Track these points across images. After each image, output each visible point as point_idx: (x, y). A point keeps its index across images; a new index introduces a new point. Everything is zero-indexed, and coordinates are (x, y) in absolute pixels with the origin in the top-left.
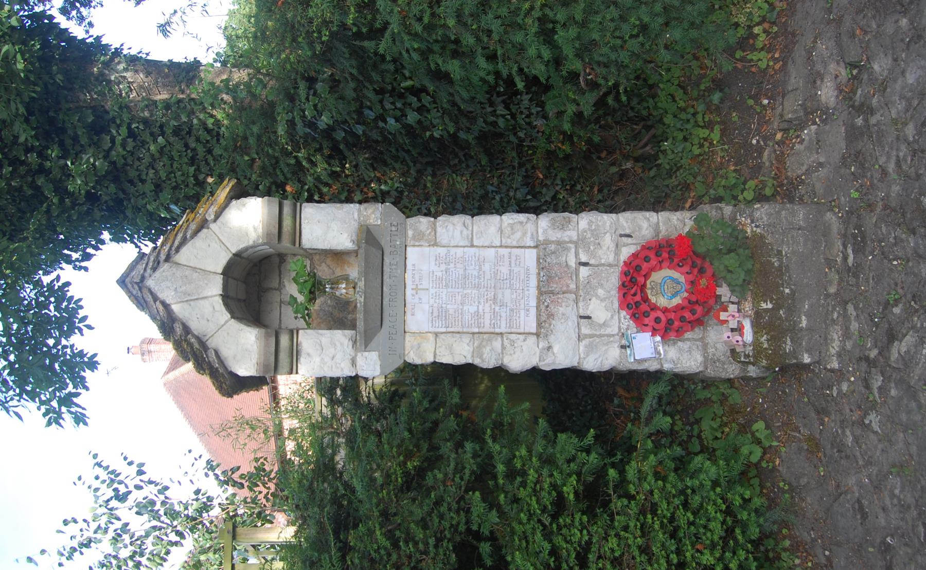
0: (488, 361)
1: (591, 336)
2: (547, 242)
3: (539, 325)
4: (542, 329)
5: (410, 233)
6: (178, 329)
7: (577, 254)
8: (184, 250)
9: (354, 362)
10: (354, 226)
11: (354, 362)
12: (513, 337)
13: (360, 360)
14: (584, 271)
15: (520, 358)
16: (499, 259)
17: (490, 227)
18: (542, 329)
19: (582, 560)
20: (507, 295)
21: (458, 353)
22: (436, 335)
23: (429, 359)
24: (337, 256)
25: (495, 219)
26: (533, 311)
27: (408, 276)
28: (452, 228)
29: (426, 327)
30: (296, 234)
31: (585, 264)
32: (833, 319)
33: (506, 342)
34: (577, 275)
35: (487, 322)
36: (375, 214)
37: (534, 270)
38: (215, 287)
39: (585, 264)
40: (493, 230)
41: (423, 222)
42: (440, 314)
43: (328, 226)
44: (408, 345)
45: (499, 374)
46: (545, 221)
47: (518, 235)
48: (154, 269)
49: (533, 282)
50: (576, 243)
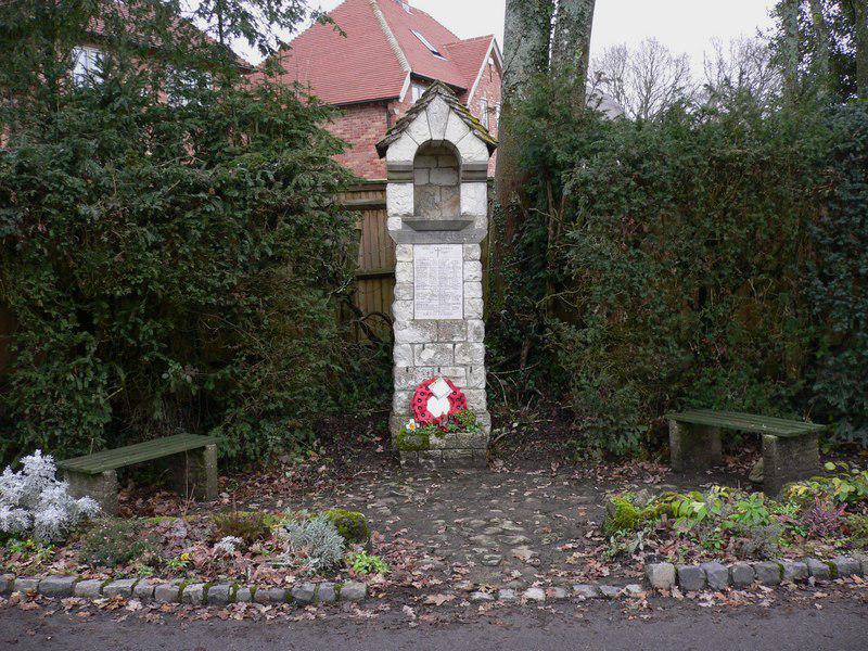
0: (399, 291)
1: (413, 350)
2: (467, 324)
3: (418, 321)
4: (415, 323)
5: (470, 246)
6: (414, 116)
7: (460, 342)
8: (457, 117)
9: (395, 215)
10: (474, 212)
11: (395, 215)
12: (412, 306)
13: (396, 219)
14: (450, 346)
15: (401, 311)
16: (457, 298)
17: (475, 292)
18: (415, 323)
19: (864, 378)
20: (435, 303)
21: (402, 276)
22: (412, 262)
23: (481, 300)
24: (457, 202)
25: (480, 294)
26: (427, 317)
27: (446, 246)
28: (474, 270)
29: (417, 257)
30: (470, 180)
31: (454, 347)
32: (511, 426)
33: (408, 302)
34: (448, 342)
35: (420, 291)
36: (481, 224)
37: (451, 317)
38: (437, 137)
39: (454, 347)
40: (473, 294)
41: (477, 253)
42: (424, 264)
43: (474, 200)
44: (406, 246)
45: (392, 299)
46: (479, 324)
47: (470, 308)
48: (445, 100)
49: (443, 317)
50: (466, 341)
